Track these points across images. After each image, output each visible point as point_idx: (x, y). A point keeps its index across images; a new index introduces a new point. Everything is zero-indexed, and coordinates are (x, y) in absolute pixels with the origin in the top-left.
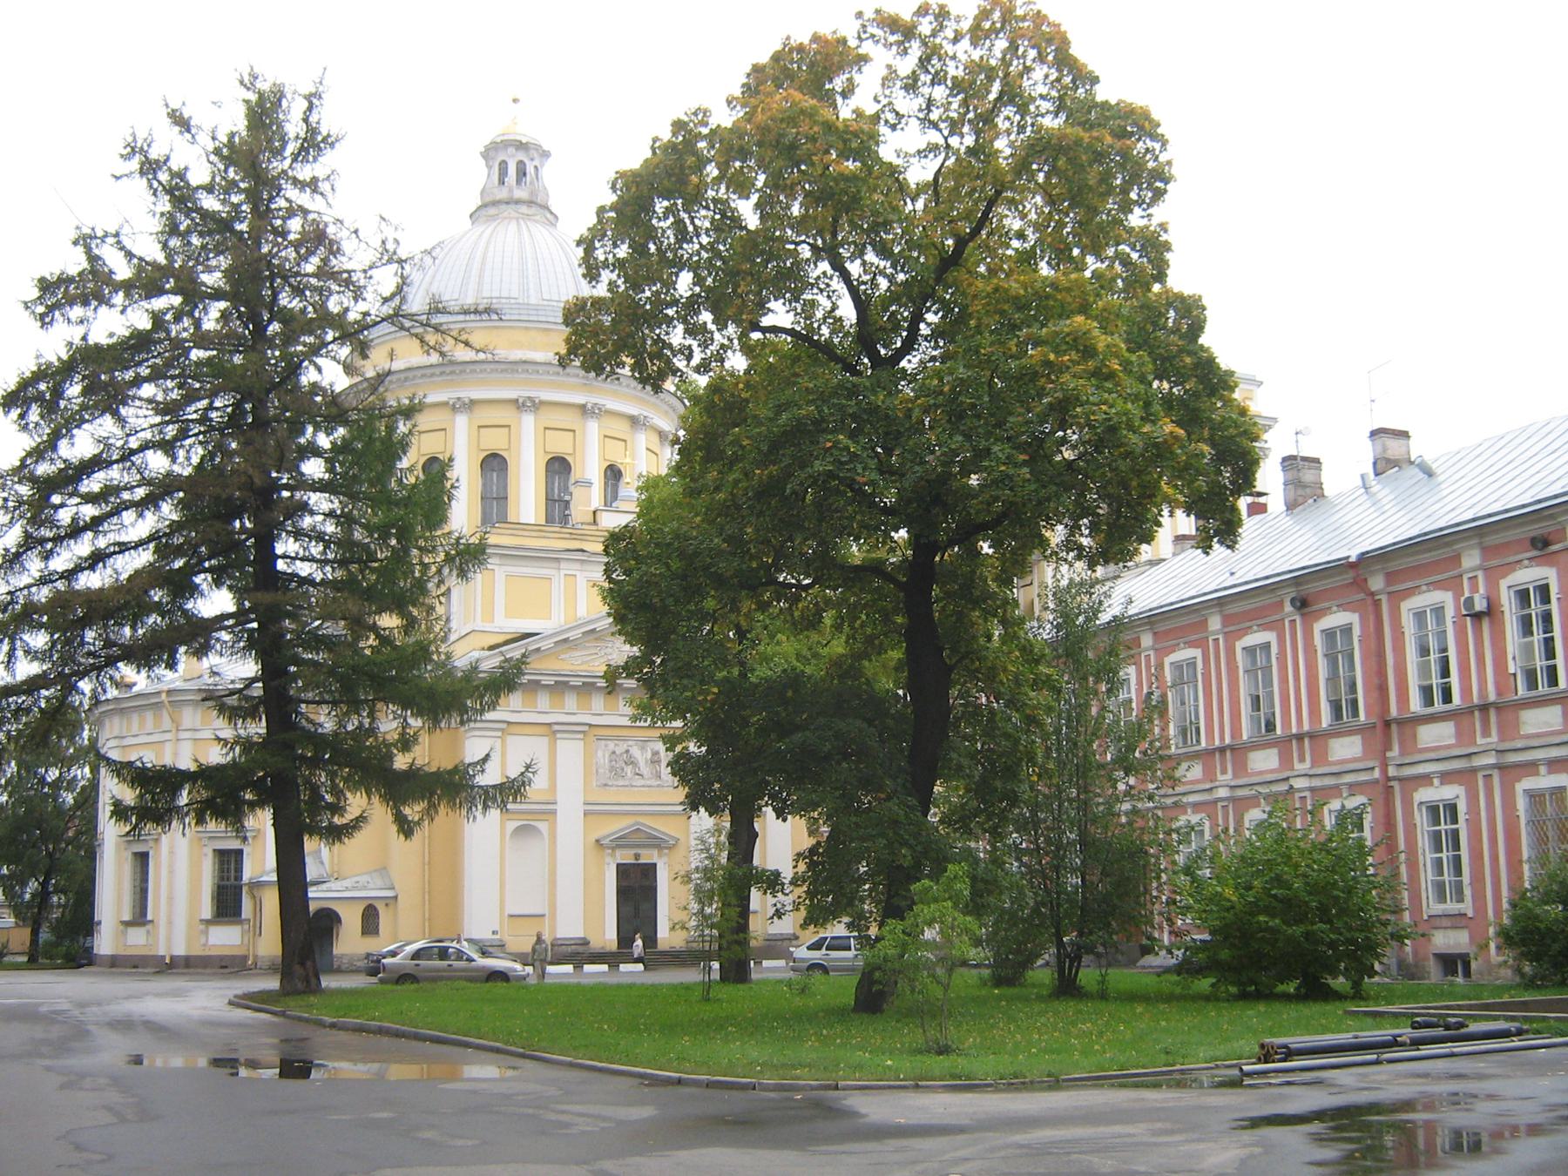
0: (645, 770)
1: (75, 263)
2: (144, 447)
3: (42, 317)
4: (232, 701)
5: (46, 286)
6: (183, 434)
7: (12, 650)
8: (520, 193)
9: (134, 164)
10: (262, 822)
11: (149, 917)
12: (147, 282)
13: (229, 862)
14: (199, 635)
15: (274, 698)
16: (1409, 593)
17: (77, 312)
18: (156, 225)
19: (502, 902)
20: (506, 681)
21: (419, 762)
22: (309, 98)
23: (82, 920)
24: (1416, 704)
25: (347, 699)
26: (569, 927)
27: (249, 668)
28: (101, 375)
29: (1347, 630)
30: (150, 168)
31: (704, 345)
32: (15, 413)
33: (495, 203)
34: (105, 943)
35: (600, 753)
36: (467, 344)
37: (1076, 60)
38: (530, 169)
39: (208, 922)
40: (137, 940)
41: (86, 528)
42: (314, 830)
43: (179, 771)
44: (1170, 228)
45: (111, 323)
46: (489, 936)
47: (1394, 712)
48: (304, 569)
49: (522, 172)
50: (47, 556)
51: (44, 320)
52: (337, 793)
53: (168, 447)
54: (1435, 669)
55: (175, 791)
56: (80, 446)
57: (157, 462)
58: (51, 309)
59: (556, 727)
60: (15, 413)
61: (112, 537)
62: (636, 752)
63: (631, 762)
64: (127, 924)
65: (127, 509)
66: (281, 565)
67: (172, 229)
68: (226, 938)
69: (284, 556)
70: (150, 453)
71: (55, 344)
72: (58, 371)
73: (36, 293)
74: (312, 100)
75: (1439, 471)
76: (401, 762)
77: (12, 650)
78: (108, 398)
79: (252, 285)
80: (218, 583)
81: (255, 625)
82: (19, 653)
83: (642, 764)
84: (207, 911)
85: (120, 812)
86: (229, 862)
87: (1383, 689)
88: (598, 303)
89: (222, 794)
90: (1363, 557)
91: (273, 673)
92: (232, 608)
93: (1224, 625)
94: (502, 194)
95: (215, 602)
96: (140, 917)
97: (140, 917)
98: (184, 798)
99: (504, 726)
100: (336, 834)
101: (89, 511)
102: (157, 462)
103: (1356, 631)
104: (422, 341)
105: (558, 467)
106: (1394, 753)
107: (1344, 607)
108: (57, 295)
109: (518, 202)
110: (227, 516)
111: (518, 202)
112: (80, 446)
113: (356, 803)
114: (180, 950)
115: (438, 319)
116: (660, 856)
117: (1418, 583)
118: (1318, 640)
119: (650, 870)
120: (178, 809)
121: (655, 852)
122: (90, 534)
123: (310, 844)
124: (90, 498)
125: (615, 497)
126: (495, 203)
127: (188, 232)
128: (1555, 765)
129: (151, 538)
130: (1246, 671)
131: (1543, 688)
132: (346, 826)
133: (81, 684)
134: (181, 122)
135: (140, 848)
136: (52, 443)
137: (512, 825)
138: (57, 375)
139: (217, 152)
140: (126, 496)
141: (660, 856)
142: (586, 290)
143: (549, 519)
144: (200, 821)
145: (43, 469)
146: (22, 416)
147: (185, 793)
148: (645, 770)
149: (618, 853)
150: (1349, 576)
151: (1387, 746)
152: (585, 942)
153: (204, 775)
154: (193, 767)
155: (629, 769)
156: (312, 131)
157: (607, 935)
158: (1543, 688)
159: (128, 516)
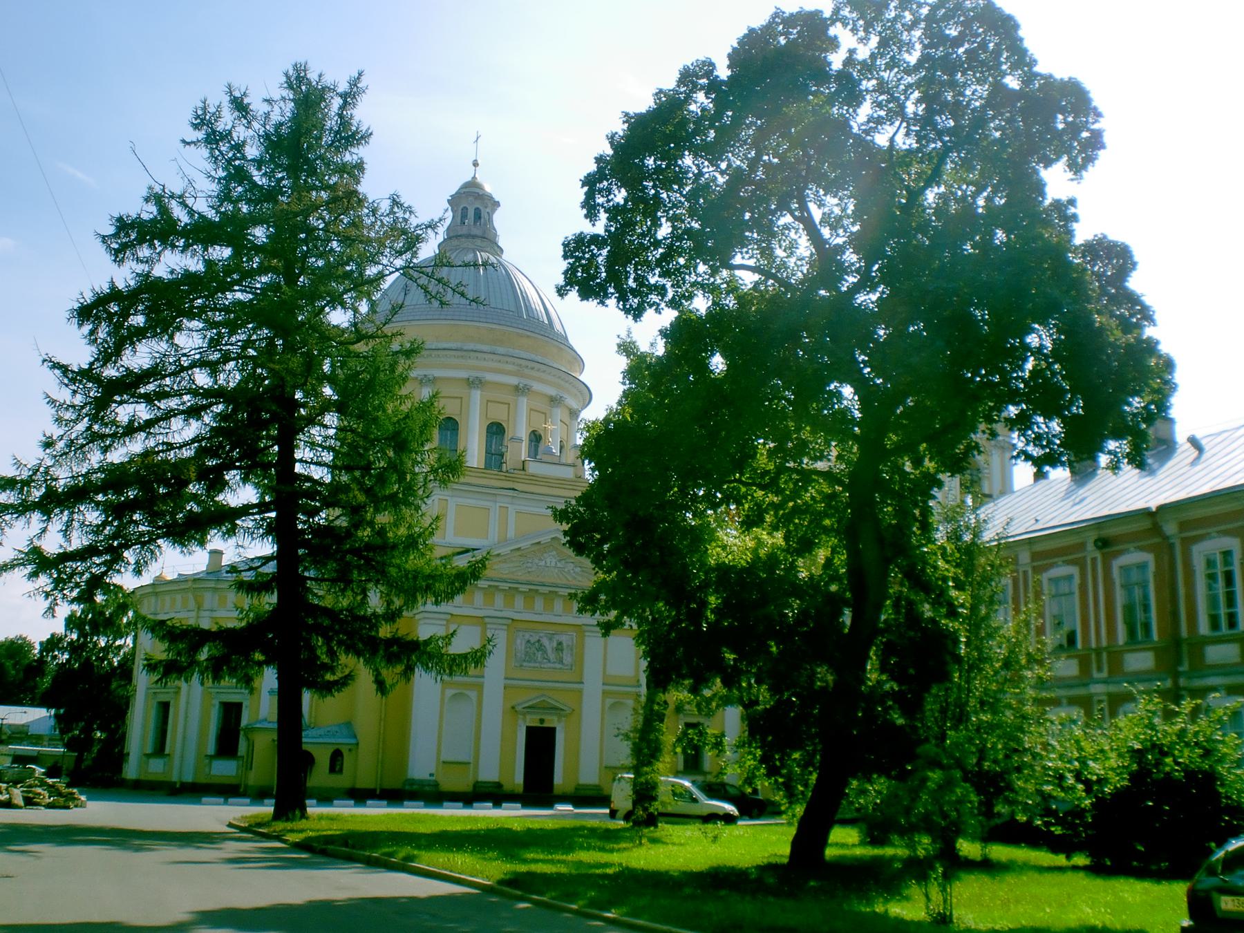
0: (552, 656)
1: (149, 212)
2: (191, 366)
3: (117, 252)
4: (248, 576)
5: (123, 225)
6: (226, 358)
7: (70, 521)
8: (475, 231)
9: (200, 135)
10: (269, 679)
11: (167, 751)
12: (202, 233)
13: (231, 712)
14: (227, 518)
15: (285, 575)
16: (1200, 538)
17: (144, 252)
18: (214, 188)
19: (439, 751)
20: (463, 581)
21: (400, 634)
22: (344, 96)
23: (113, 754)
24: (1204, 628)
25: (342, 579)
26: (489, 773)
27: (267, 548)
28: (163, 303)
29: (1142, 567)
30: (214, 138)
31: (676, 285)
32: (87, 328)
33: (458, 237)
34: (131, 771)
35: (519, 641)
36: (462, 295)
37: (1026, 51)
38: (484, 214)
39: (211, 757)
40: (156, 768)
41: (141, 428)
42: (311, 685)
43: (203, 631)
44: (1079, 204)
45: (172, 262)
46: (427, 777)
47: (1184, 633)
48: (317, 473)
49: (478, 215)
50: (105, 450)
51: (119, 255)
52: (332, 654)
53: (213, 368)
54: (1222, 599)
55: (195, 648)
56: (140, 357)
57: (202, 379)
58: (123, 248)
59: (487, 620)
60: (87, 328)
61: (161, 438)
62: (545, 642)
63: (541, 648)
64: (148, 756)
65: (175, 415)
66: (298, 468)
67: (225, 196)
68: (225, 769)
69: (301, 461)
70: (197, 370)
71: (125, 276)
72: (127, 297)
73: (111, 230)
74: (349, 98)
75: (1207, 448)
76: (385, 631)
77: (70, 521)
78: (162, 325)
79: (290, 230)
80: (245, 480)
81: (273, 515)
82: (75, 524)
83: (550, 651)
84: (211, 748)
85: (151, 667)
86: (231, 712)
87: (1175, 614)
88: (595, 239)
89: (233, 650)
90: (1162, 508)
91: (285, 556)
92: (255, 501)
93: (1033, 559)
94: (464, 231)
95: (241, 493)
96: (160, 749)
97: (160, 749)
98: (203, 655)
99: (449, 617)
100: (327, 688)
101: (143, 412)
102: (202, 379)
103: (1152, 568)
104: (426, 291)
105: (496, 431)
106: (1185, 667)
107: (1141, 549)
108: (129, 235)
109: (474, 237)
110: (255, 425)
111: (474, 237)
112: (140, 357)
113: (347, 661)
114: (189, 778)
115: (444, 272)
116: (559, 721)
117: (1209, 530)
118: (1116, 573)
119: (551, 732)
120: (198, 663)
121: (555, 718)
122: (143, 435)
123: (307, 696)
124: (149, 399)
125: (536, 454)
126: (458, 237)
127: (239, 199)
128: (1233, 691)
129: (193, 441)
130: (1122, 586)
131: (1224, 630)
132: (335, 683)
133: (126, 554)
134: (240, 106)
135: (164, 698)
136: (118, 352)
137: (450, 692)
138: (123, 299)
139: (267, 136)
140: (173, 403)
141: (559, 721)
142: (588, 228)
143: (488, 466)
144: (217, 677)
145: (110, 372)
146: (92, 332)
147: (206, 649)
148: (552, 656)
149: (528, 717)
150: (1146, 524)
151: (1179, 662)
152: (499, 785)
153: (224, 636)
154: (214, 628)
155: (539, 655)
156: (344, 122)
157: (517, 779)
158: (1224, 630)
159: (177, 423)
